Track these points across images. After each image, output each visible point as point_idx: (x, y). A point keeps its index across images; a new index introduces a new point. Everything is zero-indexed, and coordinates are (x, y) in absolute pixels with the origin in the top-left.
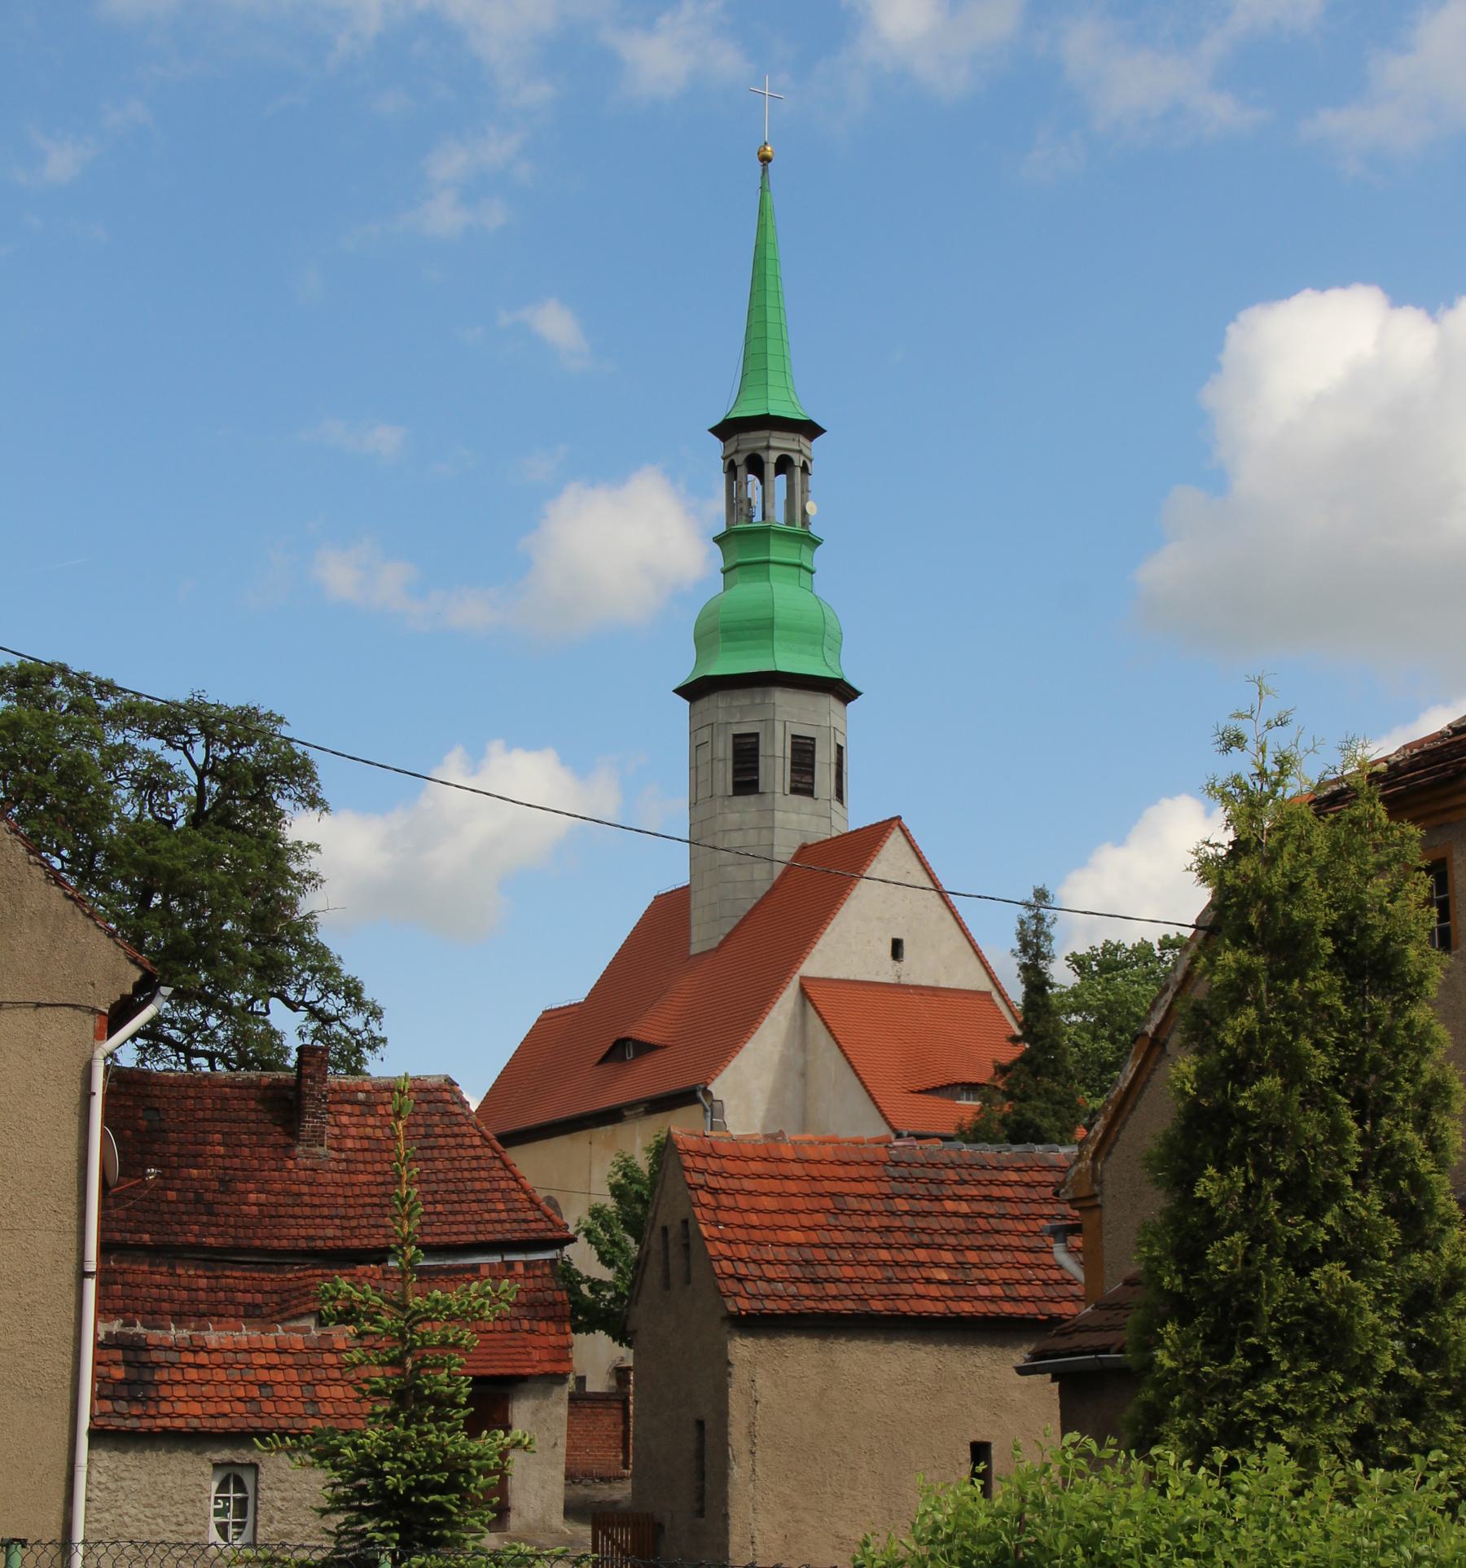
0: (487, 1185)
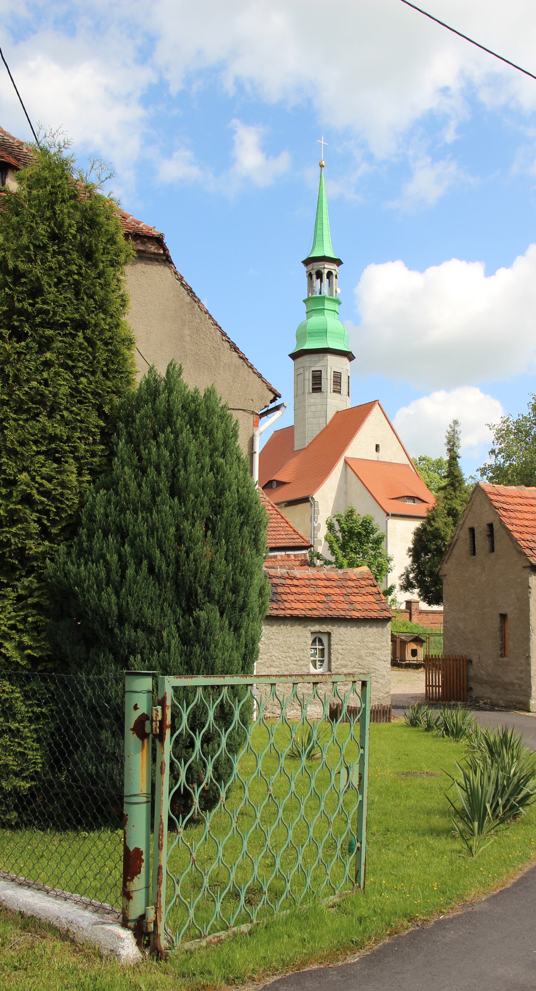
0: (276, 525)
